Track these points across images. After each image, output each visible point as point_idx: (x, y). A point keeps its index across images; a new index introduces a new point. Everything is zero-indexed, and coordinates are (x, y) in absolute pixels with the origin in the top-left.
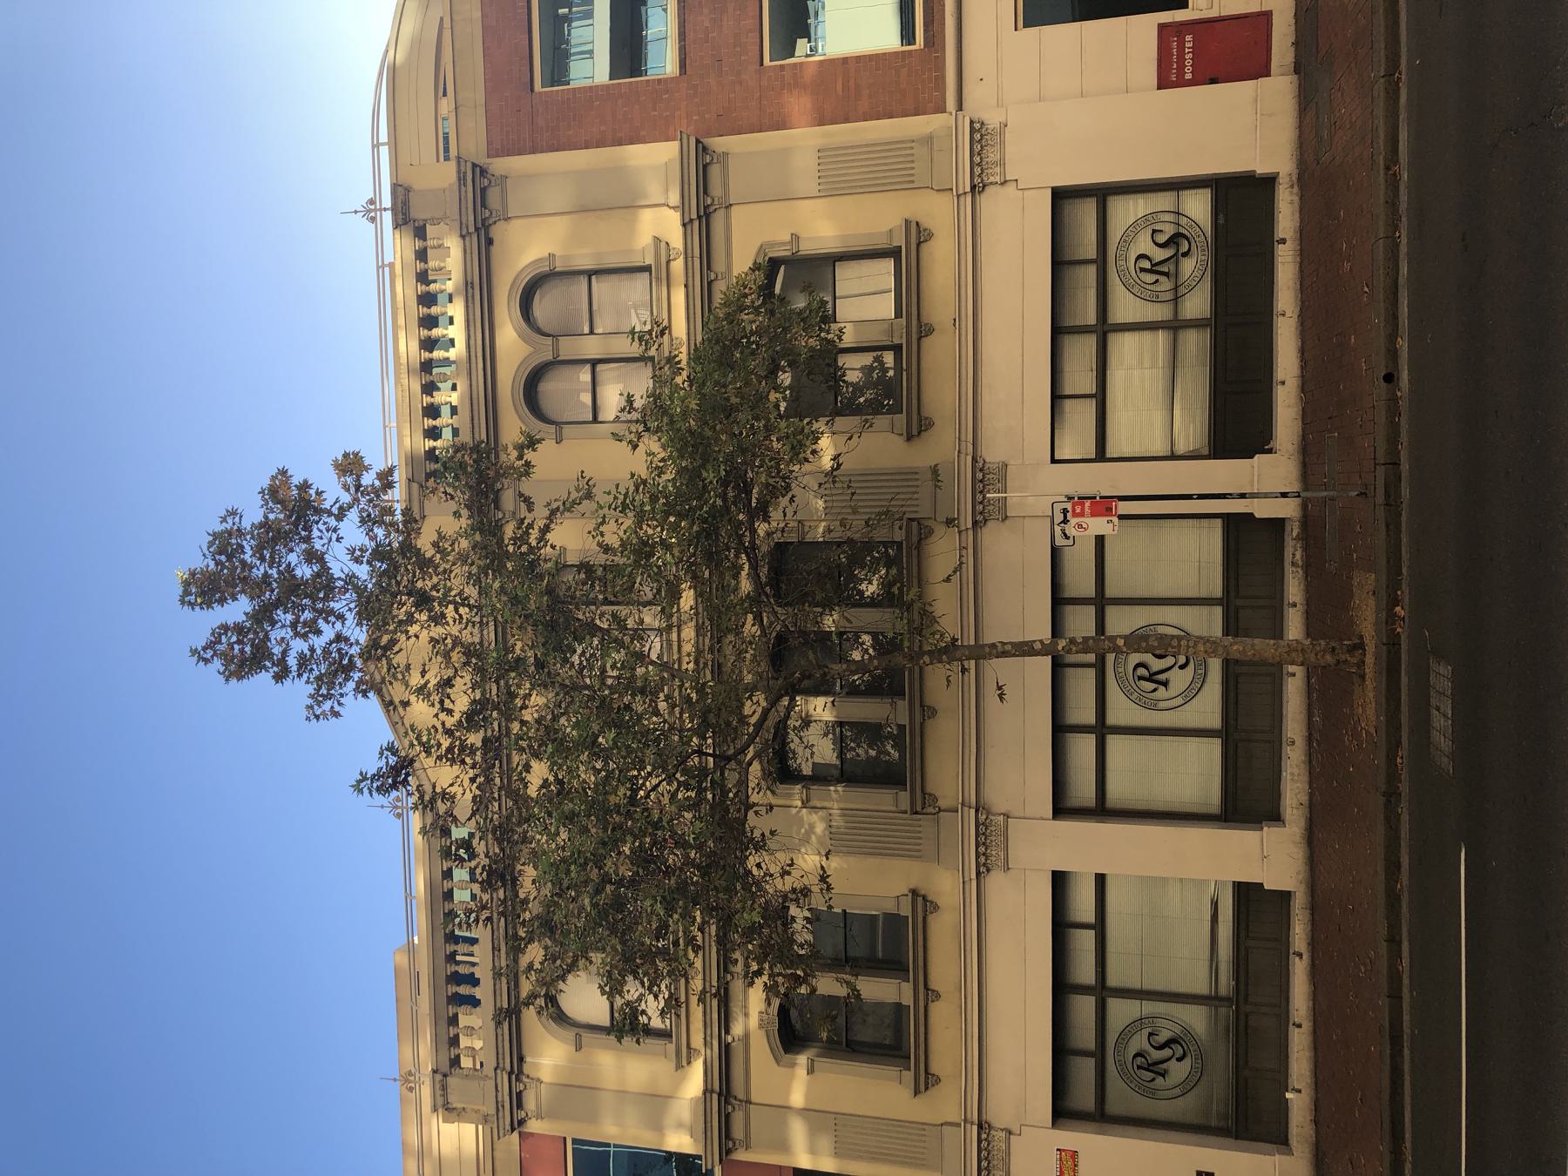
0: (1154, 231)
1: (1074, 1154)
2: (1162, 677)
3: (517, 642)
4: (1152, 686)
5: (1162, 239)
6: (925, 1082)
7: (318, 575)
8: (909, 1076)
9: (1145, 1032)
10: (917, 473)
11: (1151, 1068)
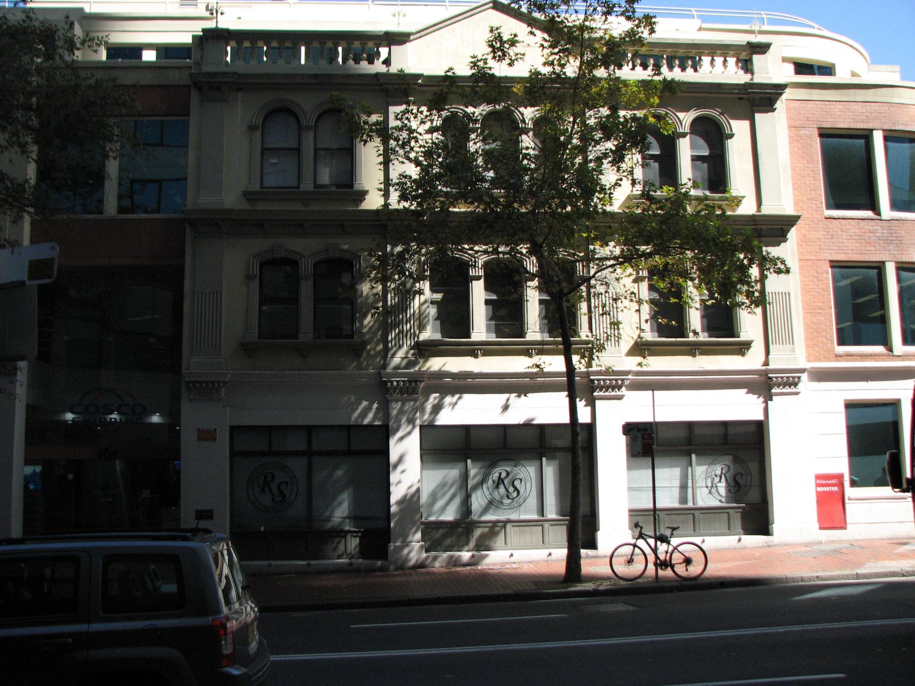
0: (287, 483)
1: (214, 439)
2: (266, 489)
3: (423, 132)
4: (261, 483)
5: (283, 488)
6: (247, 349)
7: (270, 43)
8: (254, 337)
9: (742, 471)
10: (793, 344)
11: (500, 481)
